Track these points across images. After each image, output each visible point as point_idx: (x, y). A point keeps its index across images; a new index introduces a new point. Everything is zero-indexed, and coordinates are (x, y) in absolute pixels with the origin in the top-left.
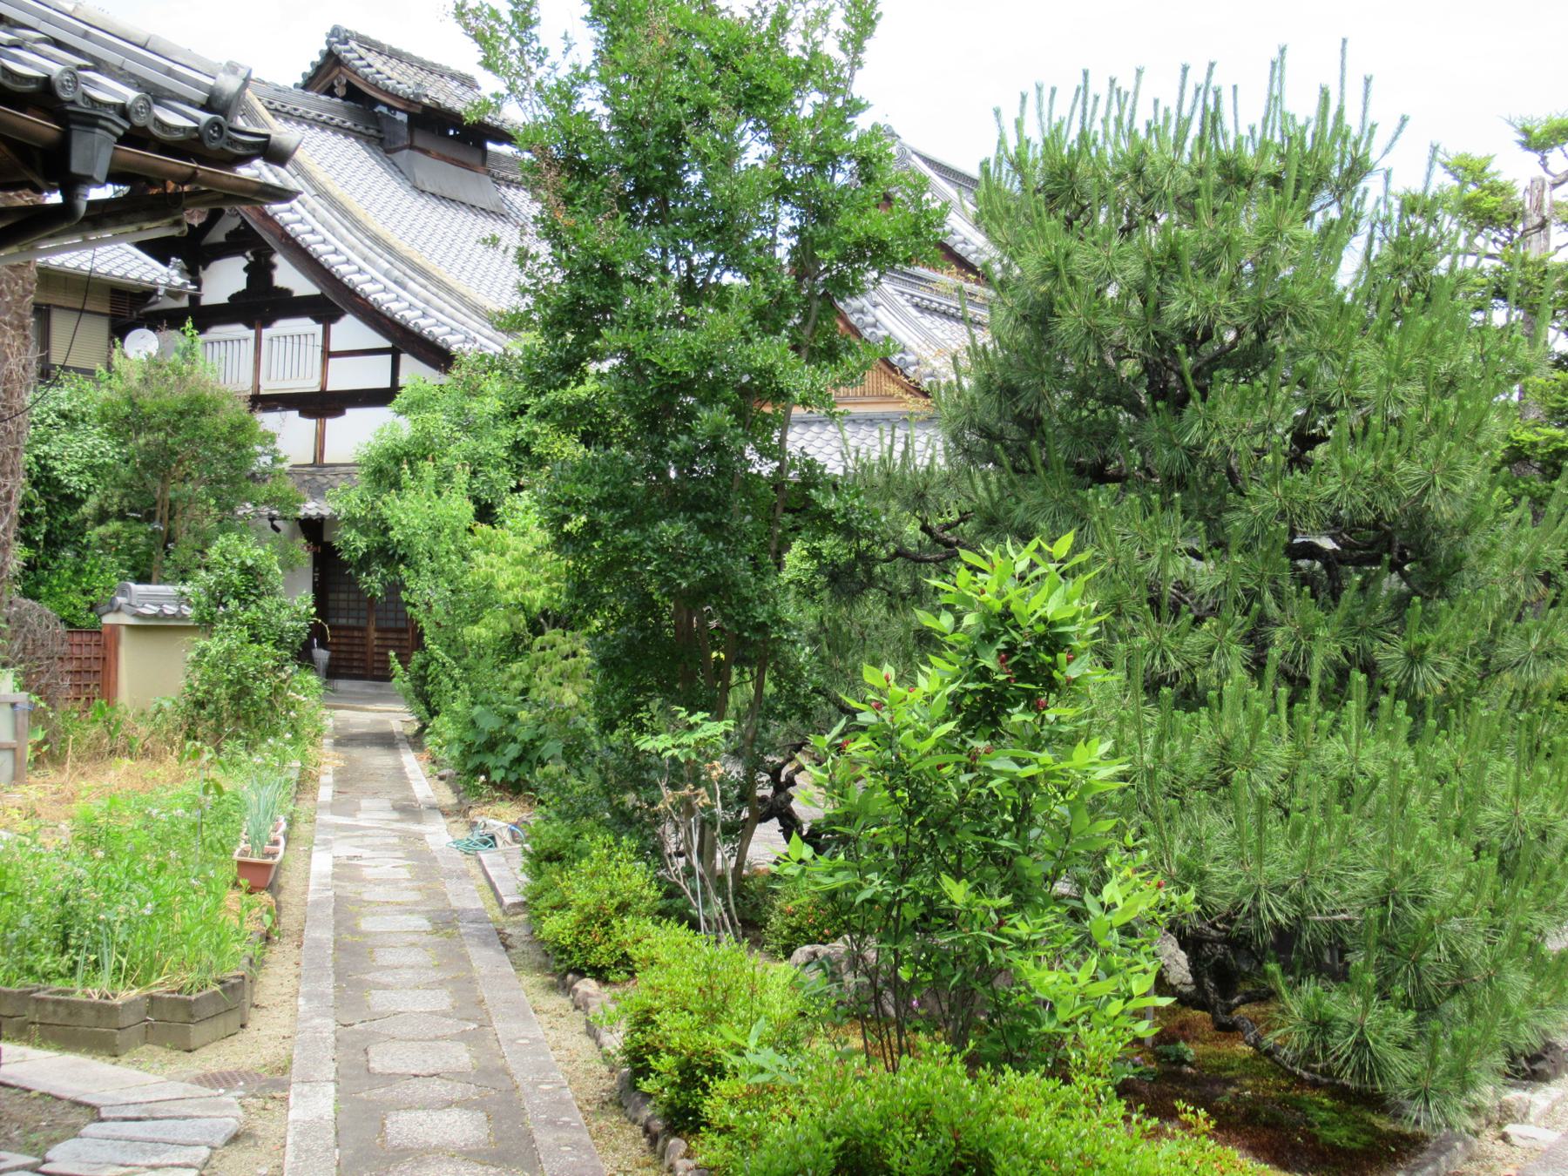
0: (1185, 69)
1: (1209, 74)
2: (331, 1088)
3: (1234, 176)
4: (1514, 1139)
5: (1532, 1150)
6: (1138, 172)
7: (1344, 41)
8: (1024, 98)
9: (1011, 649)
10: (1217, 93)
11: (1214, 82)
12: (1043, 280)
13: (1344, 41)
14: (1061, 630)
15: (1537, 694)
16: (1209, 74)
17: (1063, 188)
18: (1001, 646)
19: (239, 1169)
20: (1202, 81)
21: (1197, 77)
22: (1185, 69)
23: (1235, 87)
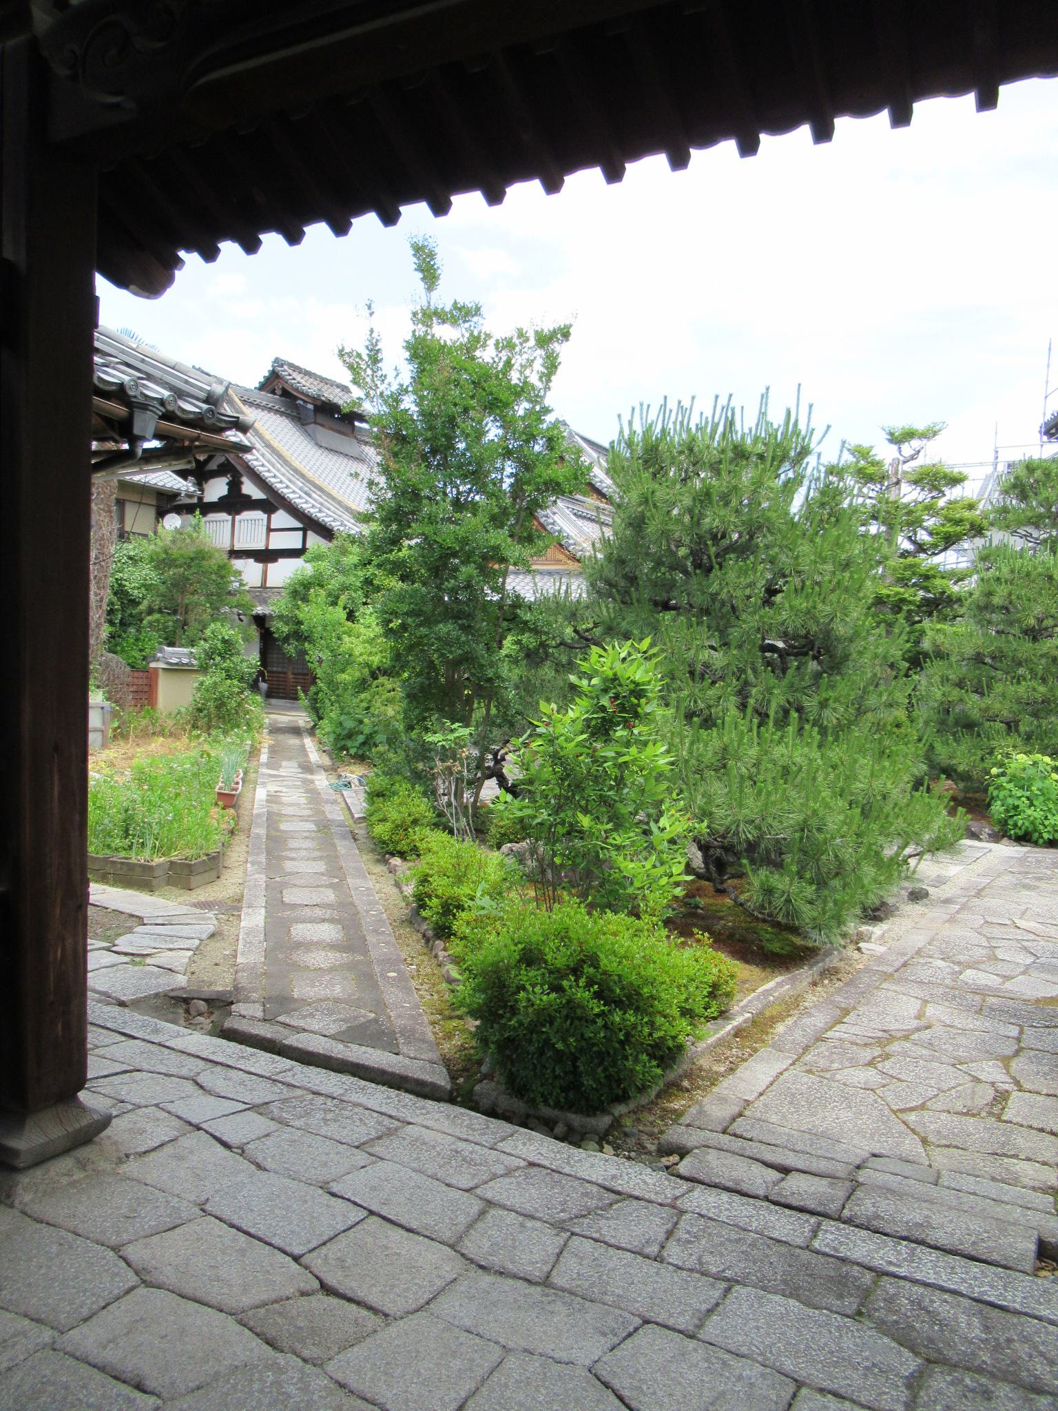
0: (717, 397)
3: (740, 454)
6: (691, 450)
10: (733, 410)
20: (725, 403)
21: (723, 401)
22: (717, 397)
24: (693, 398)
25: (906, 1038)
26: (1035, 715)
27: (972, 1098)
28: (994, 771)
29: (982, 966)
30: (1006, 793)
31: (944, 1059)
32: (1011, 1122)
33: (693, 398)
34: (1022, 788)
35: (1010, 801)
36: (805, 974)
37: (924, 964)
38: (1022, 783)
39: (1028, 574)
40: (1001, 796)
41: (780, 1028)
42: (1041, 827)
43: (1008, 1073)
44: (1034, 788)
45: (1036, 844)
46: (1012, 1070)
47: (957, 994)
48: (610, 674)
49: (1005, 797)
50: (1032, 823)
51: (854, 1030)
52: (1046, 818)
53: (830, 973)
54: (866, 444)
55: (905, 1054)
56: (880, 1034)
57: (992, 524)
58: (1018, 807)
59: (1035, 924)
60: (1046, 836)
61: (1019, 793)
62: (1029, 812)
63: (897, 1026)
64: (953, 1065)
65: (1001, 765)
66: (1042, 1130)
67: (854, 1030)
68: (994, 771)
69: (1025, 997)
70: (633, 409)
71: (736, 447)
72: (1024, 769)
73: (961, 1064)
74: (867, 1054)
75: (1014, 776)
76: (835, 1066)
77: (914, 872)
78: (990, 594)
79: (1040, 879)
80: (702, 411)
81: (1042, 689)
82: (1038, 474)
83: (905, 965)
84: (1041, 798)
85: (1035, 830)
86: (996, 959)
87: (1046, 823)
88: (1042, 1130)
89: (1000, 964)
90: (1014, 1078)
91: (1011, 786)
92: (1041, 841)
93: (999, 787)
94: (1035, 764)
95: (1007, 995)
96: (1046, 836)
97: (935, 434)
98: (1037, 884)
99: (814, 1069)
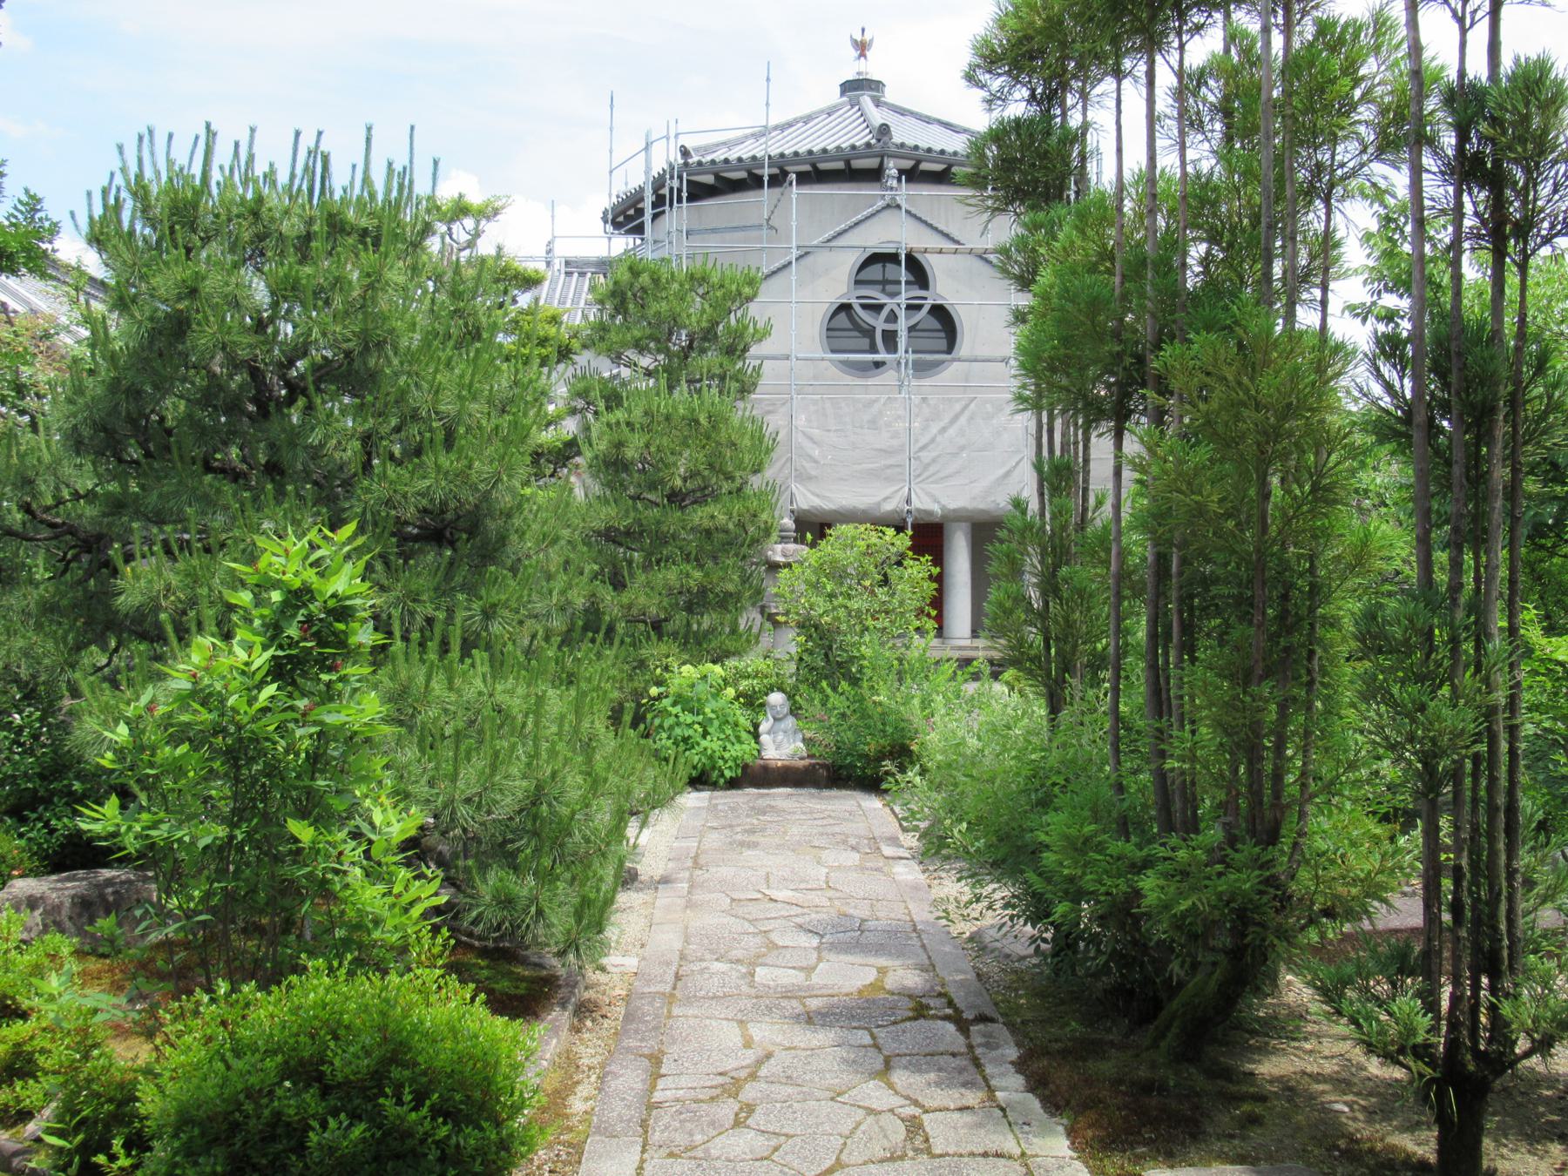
0: (298, 134)
1: (318, 142)
2: (1090, 1064)
3: (336, 226)
4: (609, 968)
5: (623, 974)
6: (256, 214)
7: (412, 128)
8: (354, 167)
9: (309, 620)
10: (326, 159)
11: (323, 147)
12: (180, 299)
13: (412, 128)
14: (348, 603)
15: (648, 638)
16: (318, 142)
17: (181, 217)
18: (300, 618)
19: (139, 1175)
20: (312, 146)
21: (307, 141)
22: (298, 134)
23: (171, 136)
24: (253, 130)
25: (753, 1076)
26: (689, 608)
27: (885, 1136)
28: (654, 691)
29: (769, 960)
30: (672, 720)
31: (818, 1094)
32: (947, 1154)
33: (253, 130)
34: (691, 711)
35: (678, 731)
36: (559, 1017)
37: (702, 971)
38: (688, 703)
39: (668, 418)
40: (666, 725)
41: (577, 1105)
42: (721, 762)
43: (897, 1093)
44: (707, 710)
45: (714, 786)
46: (899, 1088)
47: (770, 1002)
48: (297, 584)
49: (671, 728)
50: (711, 757)
51: (684, 1081)
52: (725, 749)
53: (584, 1010)
54: (40, 195)
55: (768, 1098)
56: (721, 1080)
57: (585, 347)
58: (689, 737)
59: (791, 893)
60: (728, 774)
61: (689, 718)
62: (704, 743)
63: (735, 1064)
64: (832, 1099)
65: (659, 683)
66: (985, 1155)
67: (684, 1081)
68: (654, 691)
69: (844, 991)
70: (197, 138)
71: (331, 216)
72: (693, 686)
73: (839, 1094)
74: (727, 1109)
75: (680, 696)
76: (698, 1138)
77: (635, 846)
78: (619, 445)
79: (752, 832)
80: (275, 156)
81: (698, 574)
82: (645, 279)
83: (678, 977)
84: (716, 723)
85: (713, 768)
86: (776, 947)
87: (727, 755)
88: (985, 1155)
89: (788, 954)
90: (907, 1098)
91: (678, 709)
92: (722, 781)
93: (664, 713)
94: (704, 678)
95: (825, 992)
96: (728, 774)
97: (496, 212)
98: (753, 838)
99: (676, 1151)
